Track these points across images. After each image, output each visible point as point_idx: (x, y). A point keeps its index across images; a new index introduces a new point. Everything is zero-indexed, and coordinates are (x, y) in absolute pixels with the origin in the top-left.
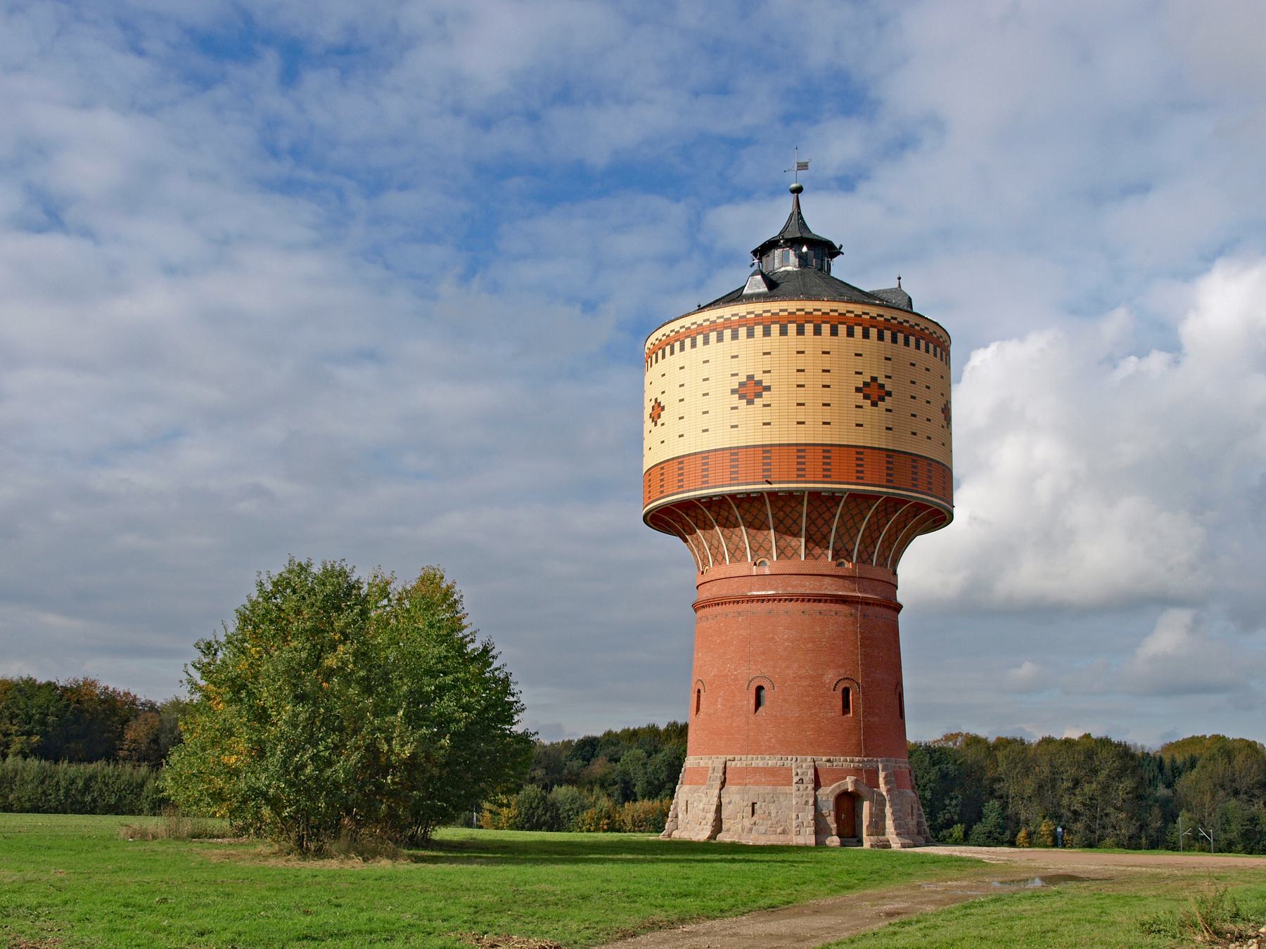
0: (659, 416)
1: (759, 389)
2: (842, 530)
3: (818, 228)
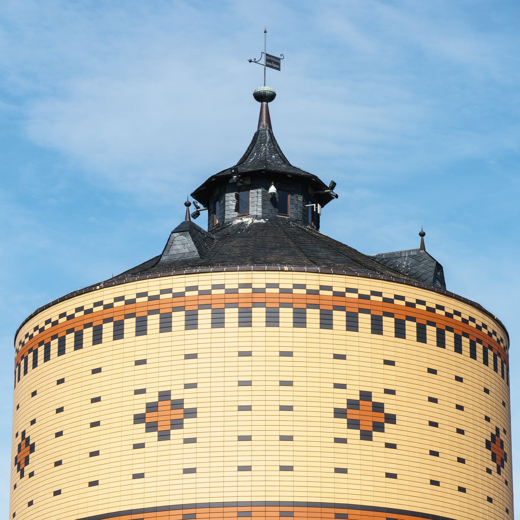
0: (27, 462)
1: (151, 417)
3: (300, 153)
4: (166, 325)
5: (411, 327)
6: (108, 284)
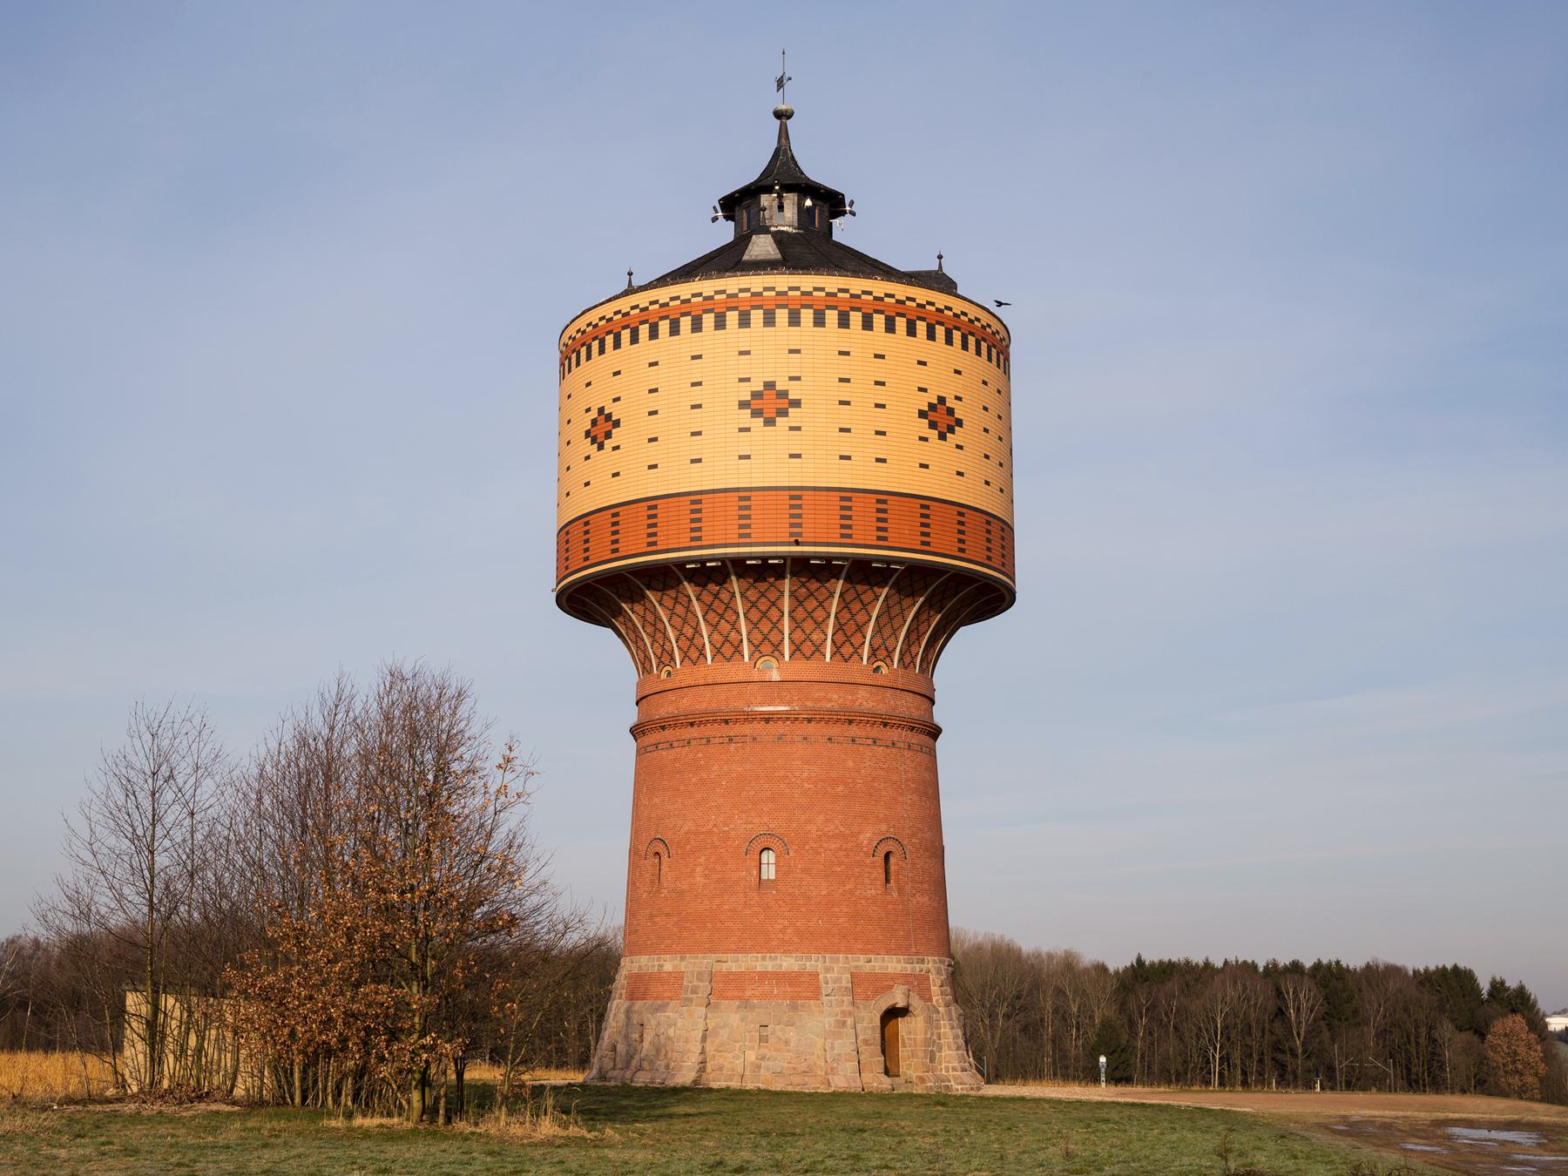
0: (608, 435)
1: (783, 403)
2: (884, 620)
3: (815, 170)
4: (720, 324)
5: (921, 327)
6: (662, 281)
